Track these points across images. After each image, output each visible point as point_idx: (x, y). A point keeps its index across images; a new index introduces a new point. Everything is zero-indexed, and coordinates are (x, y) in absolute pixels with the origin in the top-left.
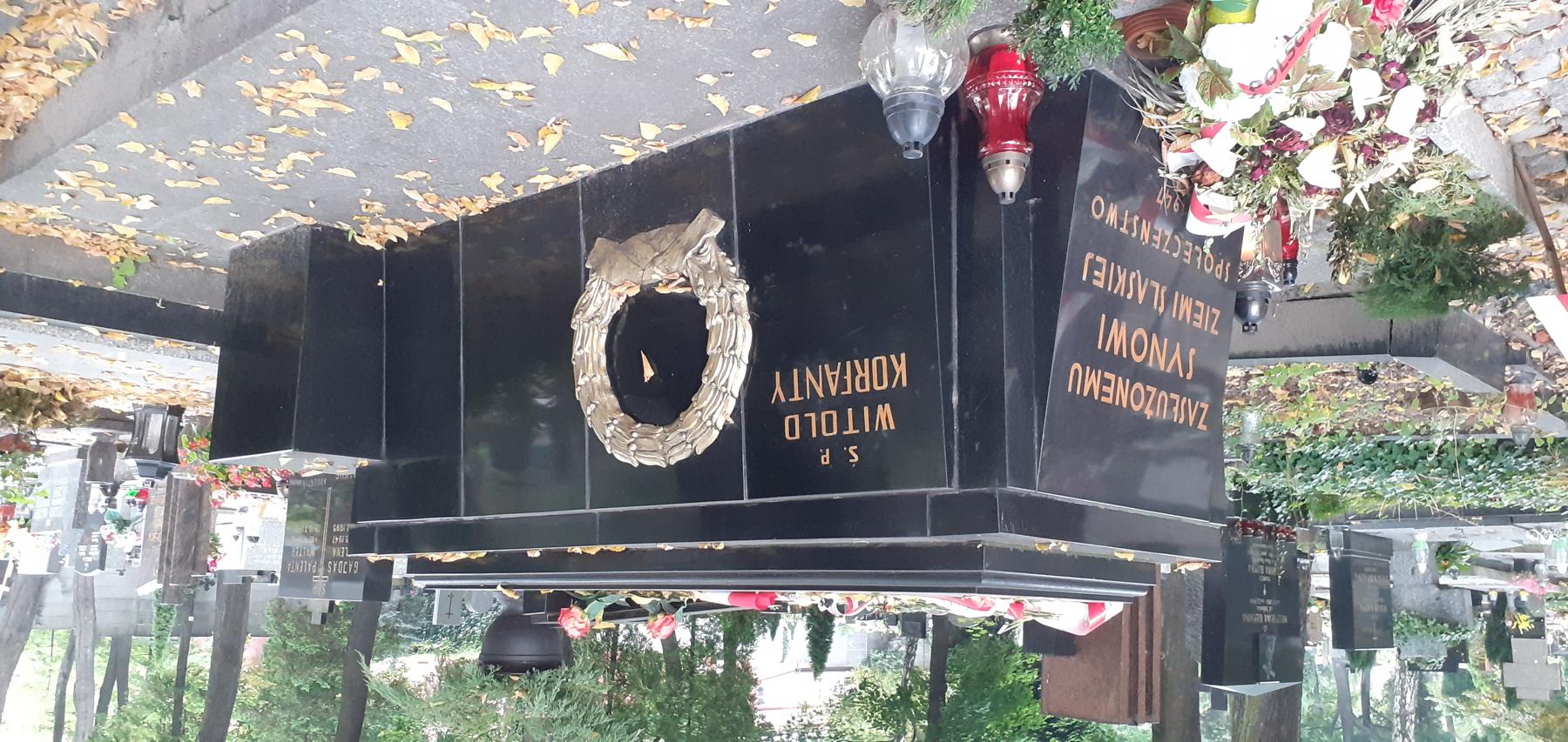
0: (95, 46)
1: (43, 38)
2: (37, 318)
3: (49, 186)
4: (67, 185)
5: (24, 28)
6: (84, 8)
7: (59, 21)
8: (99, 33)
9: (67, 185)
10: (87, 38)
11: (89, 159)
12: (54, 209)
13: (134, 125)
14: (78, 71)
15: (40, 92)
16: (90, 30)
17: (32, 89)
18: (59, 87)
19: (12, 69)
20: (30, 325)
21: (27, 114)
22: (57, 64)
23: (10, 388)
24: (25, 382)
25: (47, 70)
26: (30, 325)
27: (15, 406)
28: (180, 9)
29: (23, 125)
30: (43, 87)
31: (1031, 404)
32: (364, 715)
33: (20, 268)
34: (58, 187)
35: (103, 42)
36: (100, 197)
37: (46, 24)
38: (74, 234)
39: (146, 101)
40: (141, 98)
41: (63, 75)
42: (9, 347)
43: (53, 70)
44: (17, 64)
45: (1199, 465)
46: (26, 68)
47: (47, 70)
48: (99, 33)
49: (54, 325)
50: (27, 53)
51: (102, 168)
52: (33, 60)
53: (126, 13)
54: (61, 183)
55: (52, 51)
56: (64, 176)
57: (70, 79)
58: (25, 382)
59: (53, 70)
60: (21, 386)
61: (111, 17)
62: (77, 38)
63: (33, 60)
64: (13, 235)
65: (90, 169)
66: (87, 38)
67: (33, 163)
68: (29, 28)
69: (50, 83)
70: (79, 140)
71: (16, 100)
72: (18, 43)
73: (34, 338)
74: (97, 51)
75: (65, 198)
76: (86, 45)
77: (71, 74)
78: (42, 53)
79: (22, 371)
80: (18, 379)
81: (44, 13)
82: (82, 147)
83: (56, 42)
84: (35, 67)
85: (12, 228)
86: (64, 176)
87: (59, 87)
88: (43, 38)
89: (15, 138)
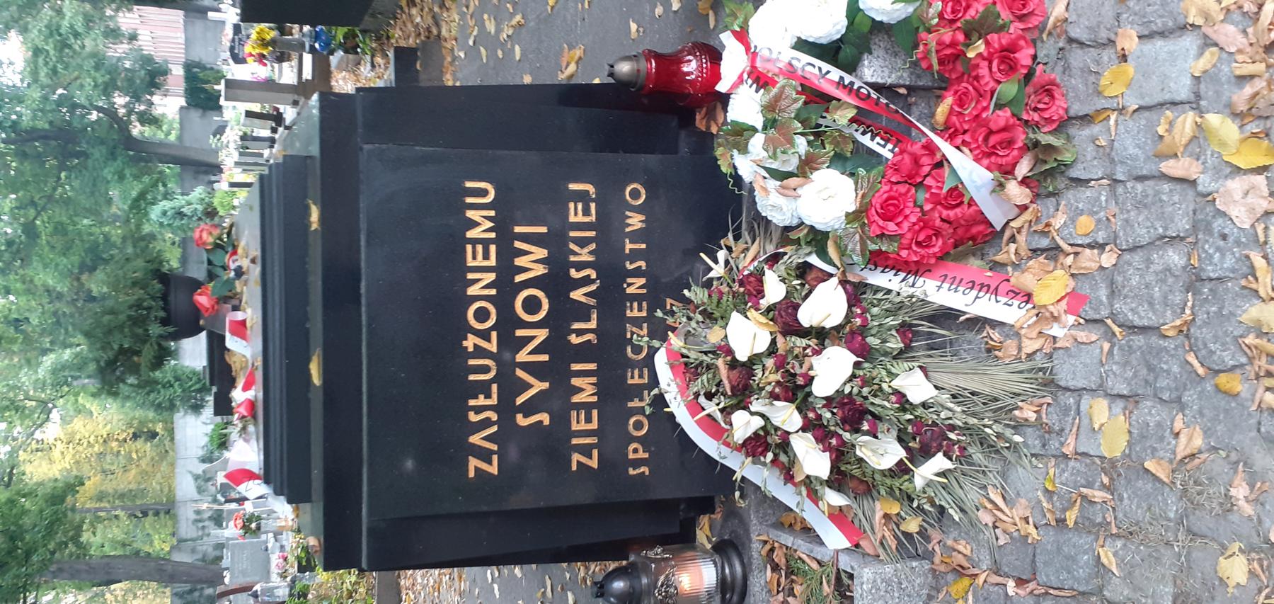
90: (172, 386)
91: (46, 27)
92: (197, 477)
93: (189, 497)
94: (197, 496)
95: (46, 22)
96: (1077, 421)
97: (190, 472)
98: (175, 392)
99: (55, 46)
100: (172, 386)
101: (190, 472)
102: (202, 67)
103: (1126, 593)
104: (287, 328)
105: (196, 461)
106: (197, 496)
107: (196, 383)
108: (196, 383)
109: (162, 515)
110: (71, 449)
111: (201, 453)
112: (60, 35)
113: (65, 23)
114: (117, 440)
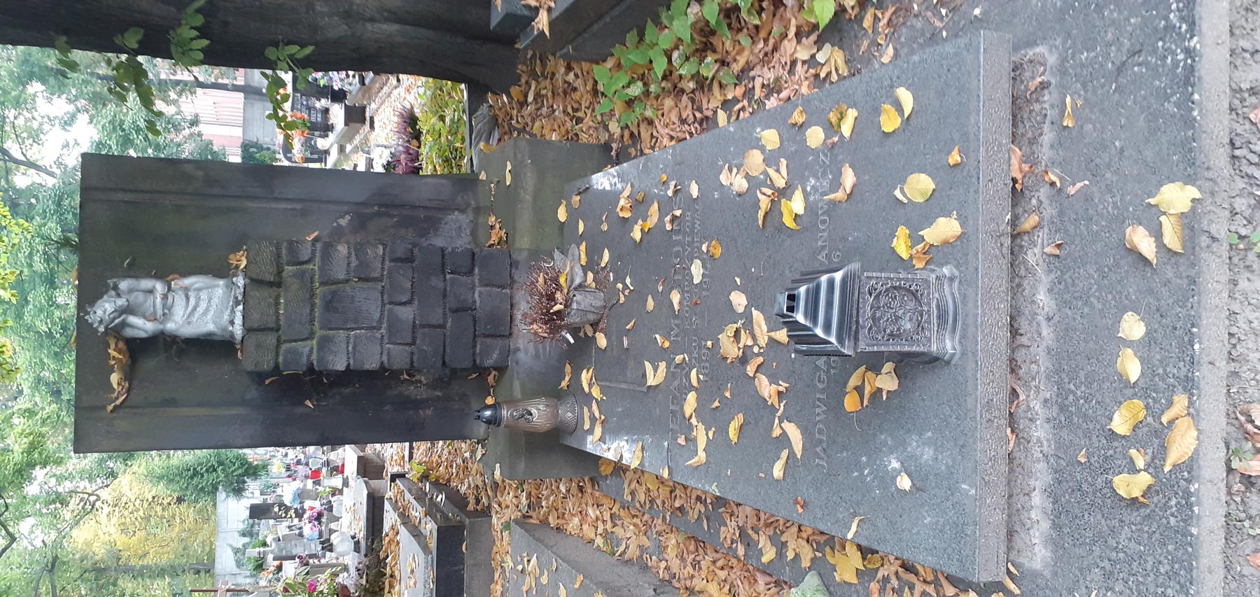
0: (624, 552)
1: (619, 522)
2: (435, 580)
3: (525, 555)
4: (528, 564)
5: (621, 510)
6: (645, 538)
7: (632, 527)
8: (633, 552)
9: (528, 564)
10: (627, 547)
11: (548, 570)
12: (511, 564)
13: (577, 586)
14: (605, 549)
15: (585, 532)
16: (633, 548)
17: (585, 527)
18: (591, 541)
19: (594, 511)
20: (429, 577)
21: (569, 529)
22: (606, 535)
23: (384, 583)
24: (389, 592)
25: (600, 530)
26: (429, 577)
27: (371, 589)
28: (663, 593)
29: (562, 530)
30: (588, 532)
31: (530, 523)
32: (81, 207)
33: (468, 561)
34: (525, 560)
35: (626, 557)
36: (525, 588)
37: (627, 520)
38: (499, 588)
39: (595, 587)
40: (596, 584)
41: (599, 541)
42: (412, 571)
43: (601, 535)
44: (598, 512)
45: (409, 341)
46: (597, 519)
47: (600, 530)
48: (633, 552)
49: (432, 593)
50: (607, 516)
51: (544, 580)
52: (604, 521)
53: (650, 564)
54: (529, 561)
55: (613, 530)
56: (534, 560)
57: (599, 546)
58: (389, 592)
59: (601, 535)
60: (387, 590)
61: (644, 556)
62: (624, 542)
63: (604, 521)
64: (490, 553)
65: (541, 574)
66: (627, 547)
67: (538, 540)
68: (622, 513)
69: (593, 536)
70: (558, 559)
71: (576, 520)
72: (611, 509)
73: (420, 585)
74: (619, 556)
75: (520, 568)
76: (622, 549)
77: (601, 546)
78: (609, 525)
79: (397, 588)
80: (391, 586)
81: (634, 516)
82: (554, 562)
83: (619, 531)
84: (600, 523)
85: (495, 549)
86: (534, 560)
87: (591, 541)
88: (619, 522)
89: (552, 528)
90: (215, 470)
91: (110, 122)
92: (236, 551)
93: (228, 570)
94: (236, 571)
95: (110, 118)
96: (350, 348)
97: (231, 546)
98: (217, 478)
99: (117, 141)
100: (215, 470)
101: (231, 546)
102: (260, 148)
103: (53, 225)
104: (200, 274)
105: (237, 535)
106: (236, 571)
107: (239, 468)
108: (239, 468)
109: (202, 574)
110: (116, 513)
111: (241, 526)
112: (123, 130)
113: (129, 119)
114: (161, 504)
